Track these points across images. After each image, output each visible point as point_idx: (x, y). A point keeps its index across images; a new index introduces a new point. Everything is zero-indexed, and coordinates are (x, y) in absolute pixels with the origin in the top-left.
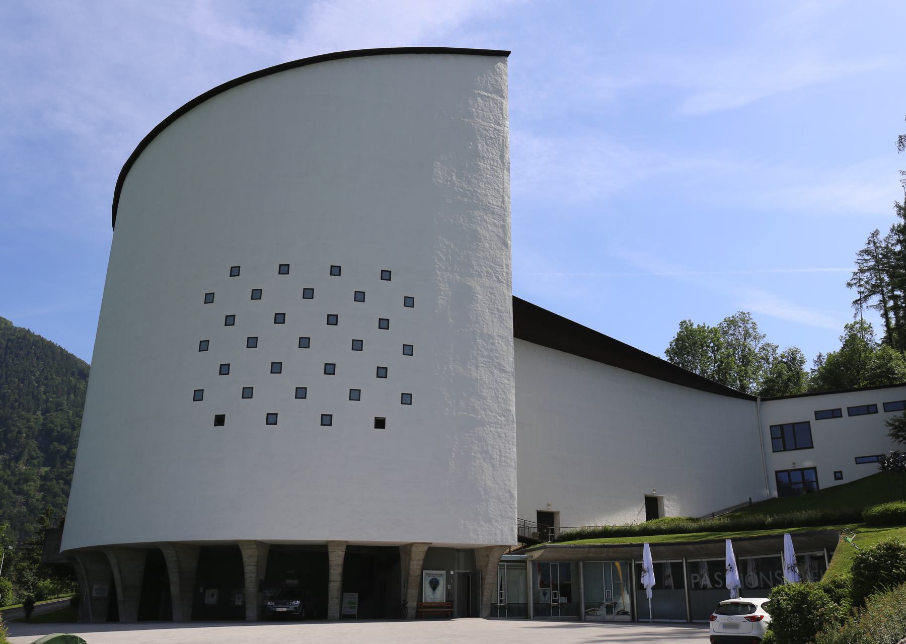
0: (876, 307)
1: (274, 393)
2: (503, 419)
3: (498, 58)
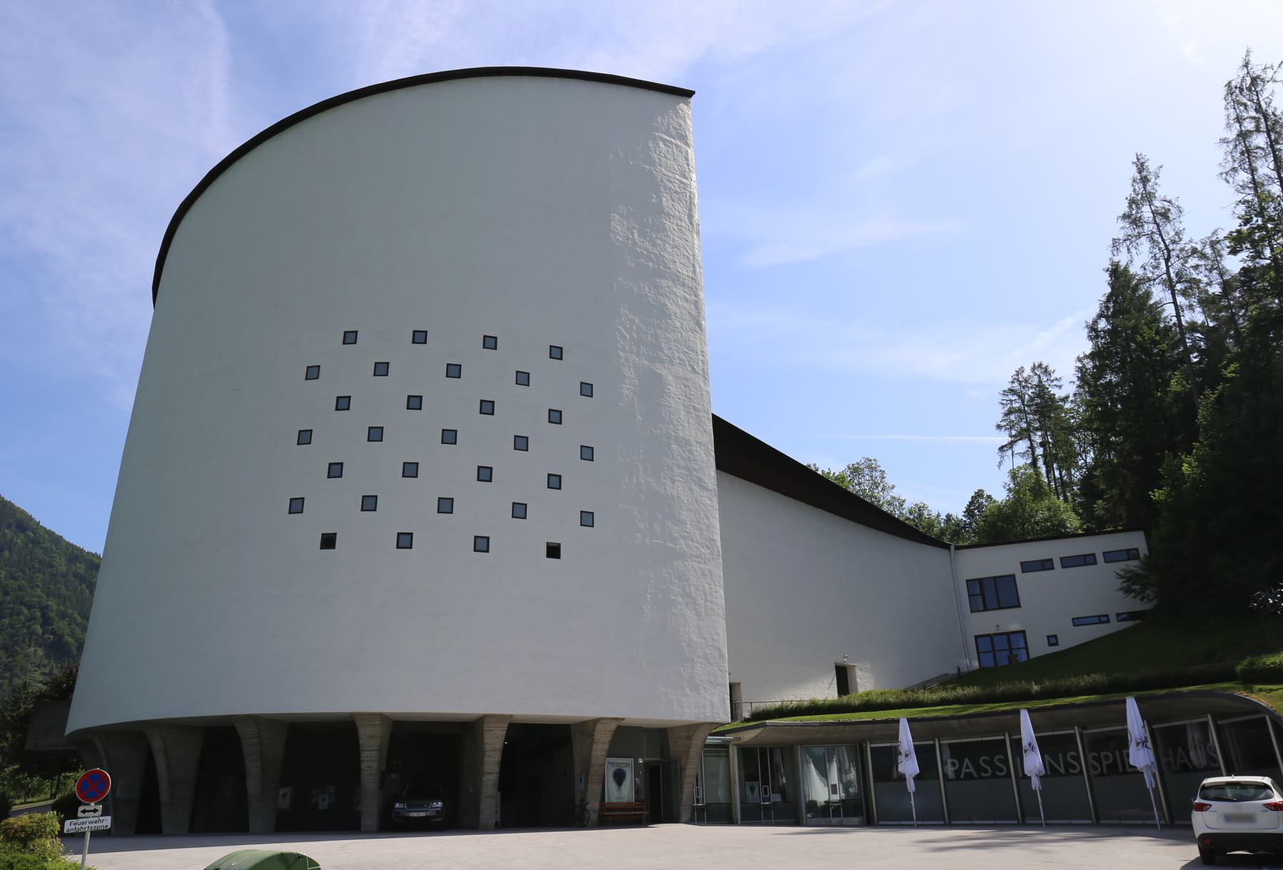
0: (1023, 455)
1: (407, 505)
2: (706, 551)
3: (680, 98)
